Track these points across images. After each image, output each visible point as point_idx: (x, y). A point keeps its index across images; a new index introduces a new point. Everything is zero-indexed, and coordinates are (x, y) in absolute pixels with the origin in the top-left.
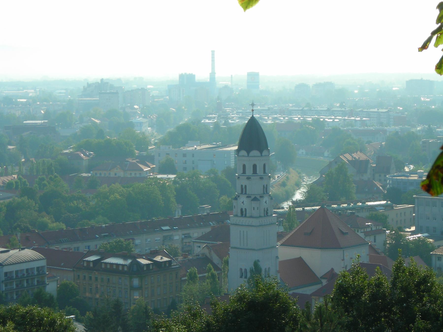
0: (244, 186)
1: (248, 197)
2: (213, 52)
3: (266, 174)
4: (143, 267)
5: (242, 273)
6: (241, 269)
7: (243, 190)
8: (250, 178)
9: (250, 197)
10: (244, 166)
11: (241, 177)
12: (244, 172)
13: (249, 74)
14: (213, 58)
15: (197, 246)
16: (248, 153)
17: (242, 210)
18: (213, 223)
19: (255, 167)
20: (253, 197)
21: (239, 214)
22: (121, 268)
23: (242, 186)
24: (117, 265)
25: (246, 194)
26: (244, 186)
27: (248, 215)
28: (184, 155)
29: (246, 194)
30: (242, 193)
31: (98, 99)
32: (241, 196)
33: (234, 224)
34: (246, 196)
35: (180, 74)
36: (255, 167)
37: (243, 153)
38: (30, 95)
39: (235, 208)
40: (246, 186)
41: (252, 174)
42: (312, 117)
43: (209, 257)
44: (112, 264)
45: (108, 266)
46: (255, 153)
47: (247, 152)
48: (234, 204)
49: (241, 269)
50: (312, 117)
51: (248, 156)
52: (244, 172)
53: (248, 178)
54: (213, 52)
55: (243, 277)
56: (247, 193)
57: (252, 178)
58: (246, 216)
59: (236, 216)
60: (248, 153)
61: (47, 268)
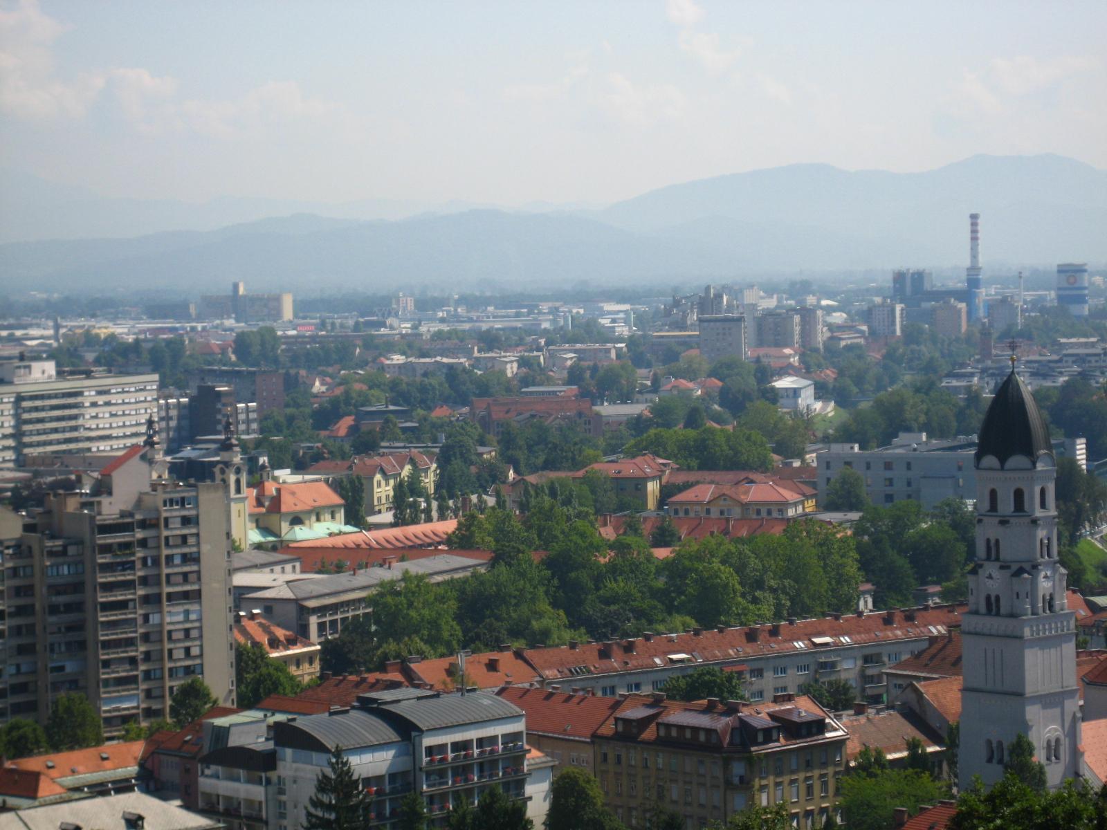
0: (993, 542)
1: (1002, 567)
2: (974, 217)
3: (1024, 514)
4: (756, 735)
5: (993, 752)
6: (989, 743)
7: (993, 550)
8: (1007, 522)
9: (1008, 567)
10: (993, 493)
11: (986, 519)
12: (993, 506)
13: (1064, 270)
14: (974, 231)
15: (895, 685)
16: (1003, 461)
17: (988, 598)
18: (937, 629)
19: (1019, 495)
20: (1015, 567)
21: (983, 609)
22: (702, 737)
23: (988, 541)
24: (695, 730)
25: (997, 559)
26: (993, 542)
27: (1002, 611)
28: (888, 466)
29: (997, 559)
30: (988, 558)
31: (698, 333)
32: (986, 564)
33: (970, 633)
34: (998, 564)
35: (896, 271)
36: (1019, 495)
37: (990, 460)
38: (543, 327)
39: (972, 594)
40: (997, 541)
41: (989, 511)
42: (578, 346)
43: (918, 711)
44: (681, 728)
45: (674, 733)
46: (1017, 460)
47: (999, 460)
48: (971, 585)
49: (989, 743)
50: (578, 346)
51: (1002, 468)
52: (993, 506)
53: (1004, 522)
54: (974, 217)
55: (995, 761)
56: (1001, 557)
57: (1012, 520)
58: (998, 614)
59: (976, 613)
60: (1003, 461)
61: (527, 734)
